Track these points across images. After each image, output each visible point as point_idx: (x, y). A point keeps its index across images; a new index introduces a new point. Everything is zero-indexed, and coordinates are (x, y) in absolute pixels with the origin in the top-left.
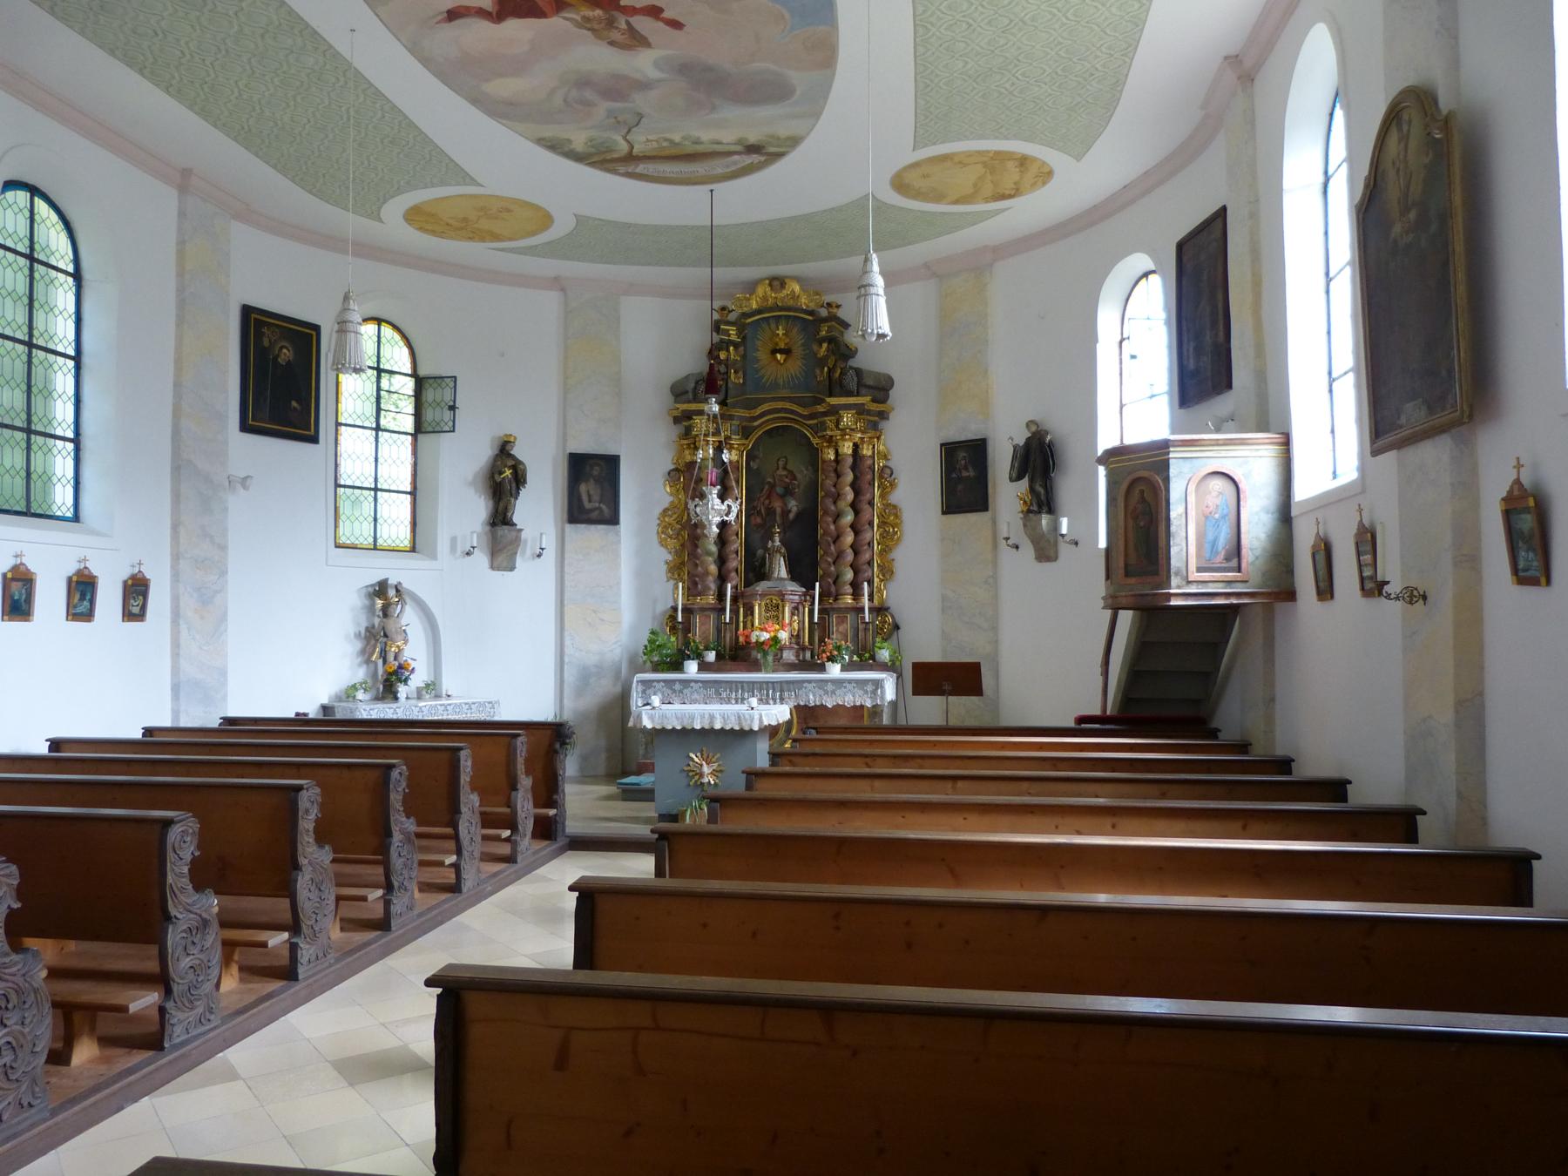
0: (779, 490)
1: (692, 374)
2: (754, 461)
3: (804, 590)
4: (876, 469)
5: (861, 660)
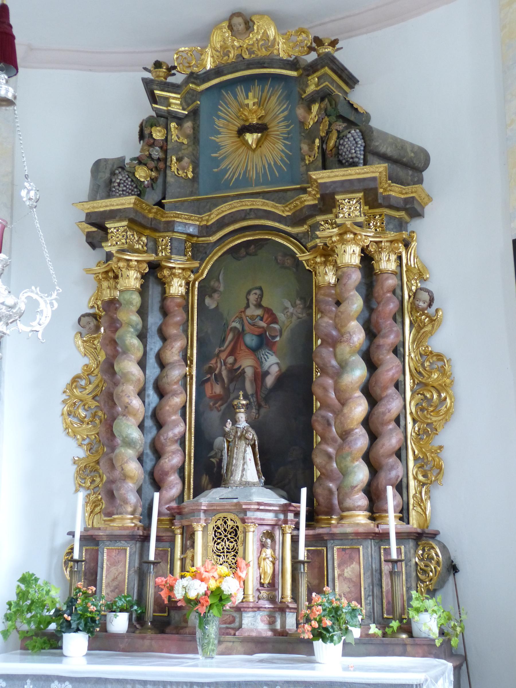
0: (250, 340)
1: (106, 160)
2: (211, 296)
3: (283, 501)
4: (406, 297)
5: (384, 635)
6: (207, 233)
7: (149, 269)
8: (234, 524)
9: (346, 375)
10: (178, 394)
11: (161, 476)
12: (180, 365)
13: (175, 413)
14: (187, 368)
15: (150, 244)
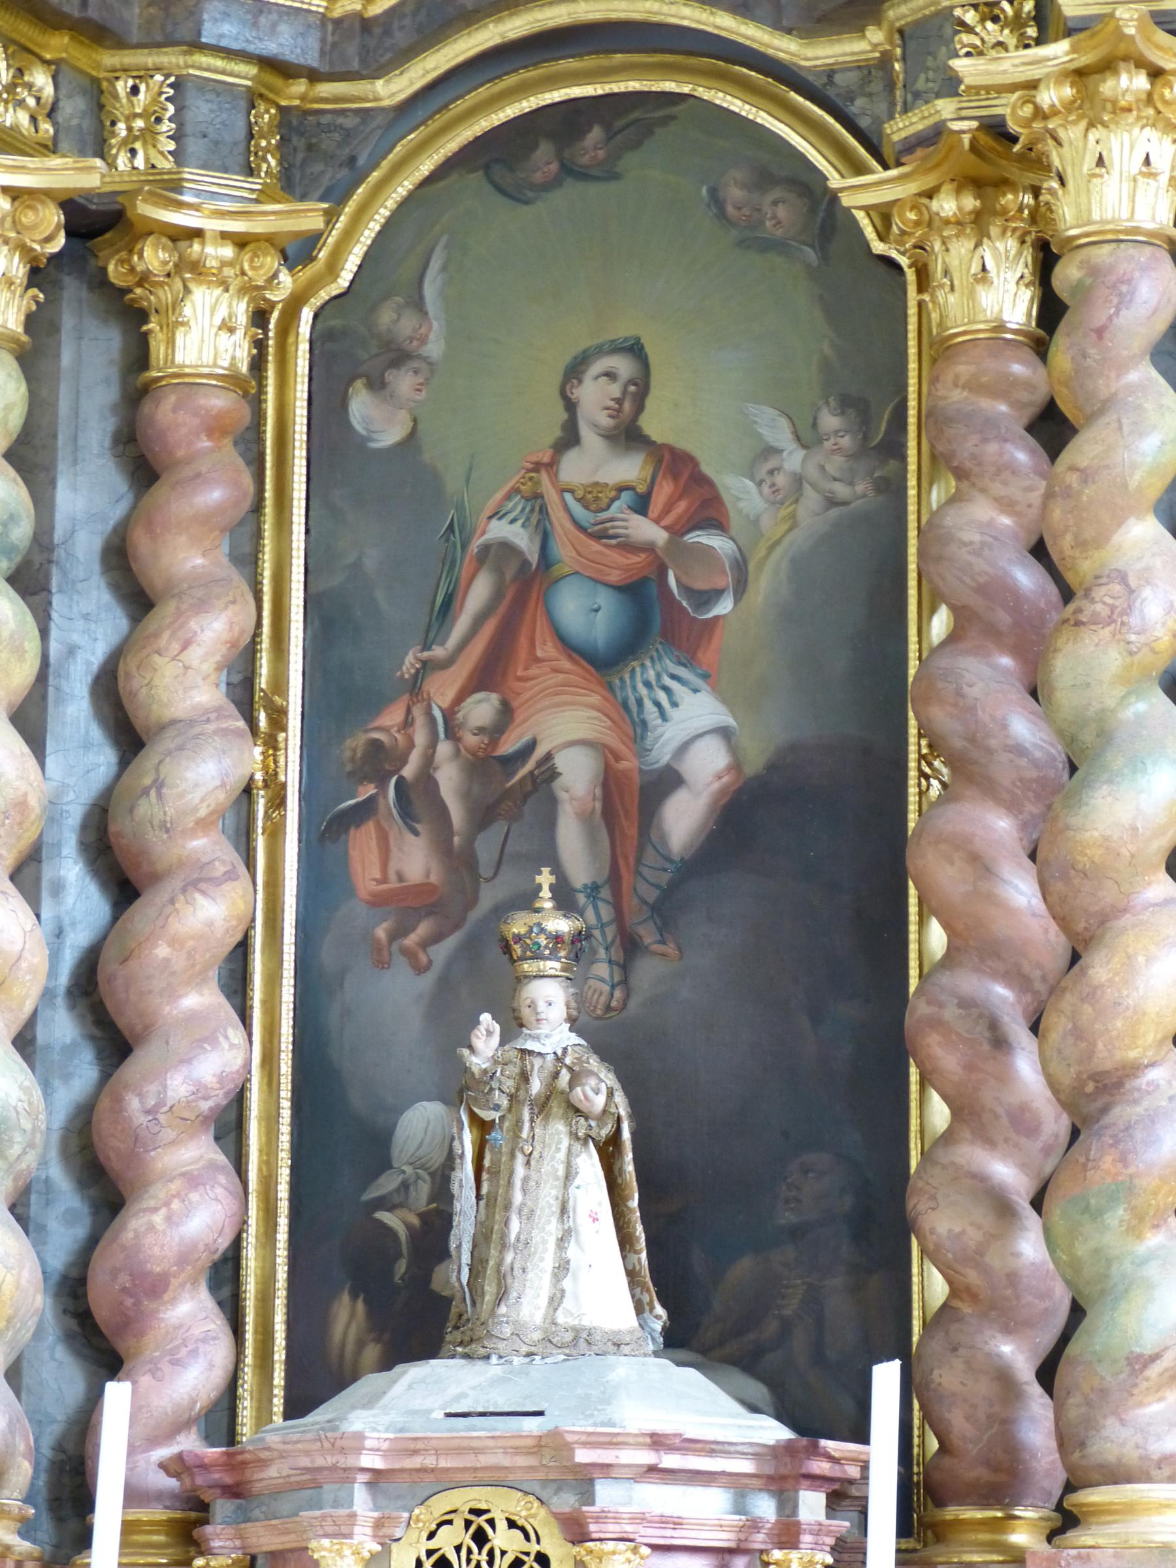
2: (377, 385)
3: (774, 1432)
6: (365, 54)
7: (69, 234)
8: (526, 1546)
9: (1105, 789)
10: (217, 882)
11: (129, 1302)
12: (225, 732)
13: (196, 980)
14: (258, 750)
15: (73, 108)
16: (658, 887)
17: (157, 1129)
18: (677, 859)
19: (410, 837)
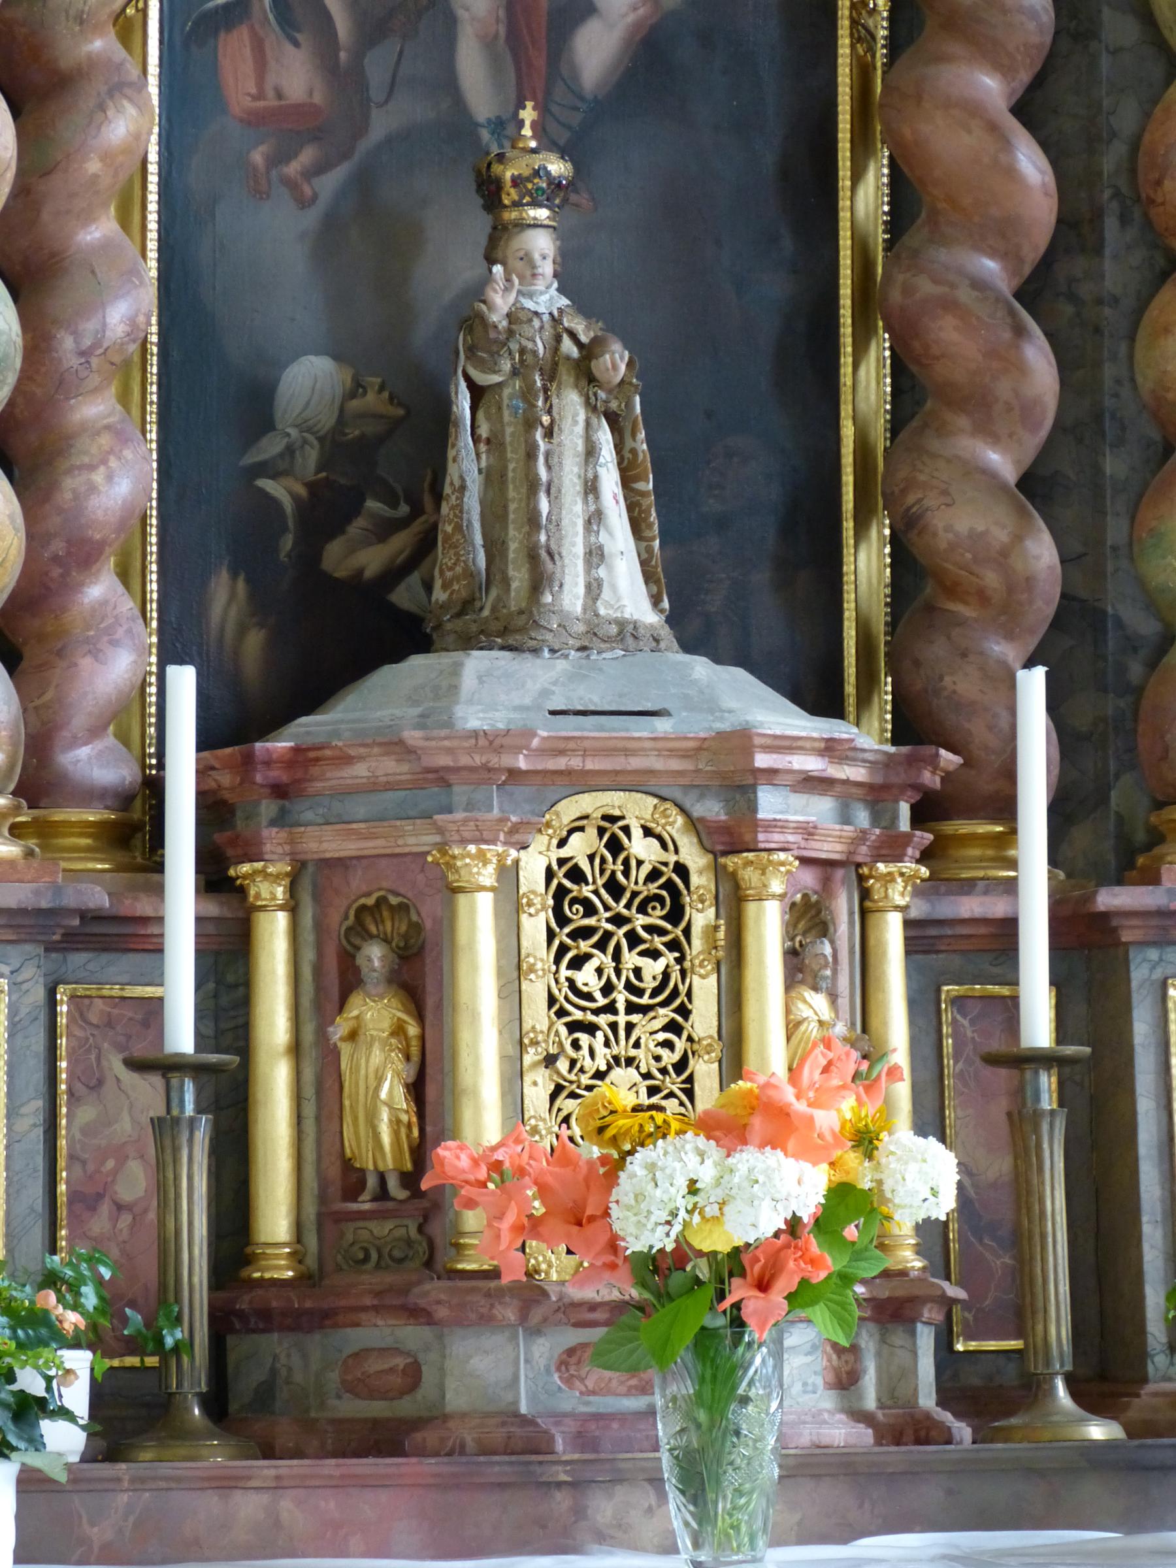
11: (56, 572)
16: (569, 127)
17: (86, 373)
18: (589, 97)
19: (289, 47)
